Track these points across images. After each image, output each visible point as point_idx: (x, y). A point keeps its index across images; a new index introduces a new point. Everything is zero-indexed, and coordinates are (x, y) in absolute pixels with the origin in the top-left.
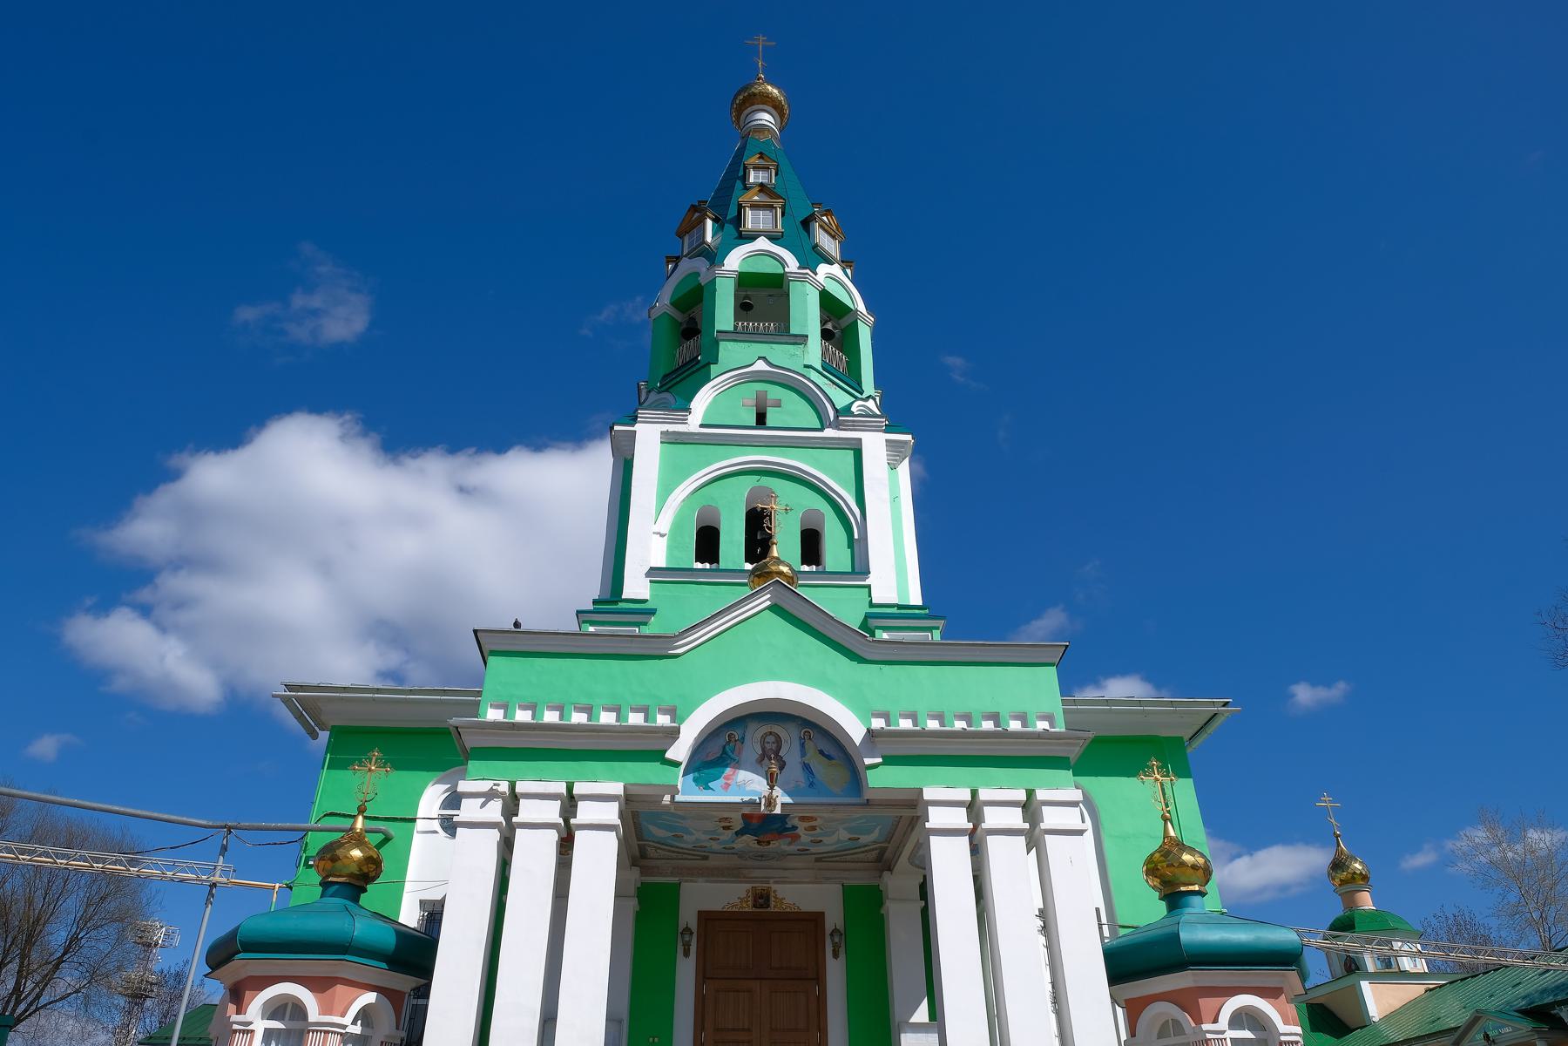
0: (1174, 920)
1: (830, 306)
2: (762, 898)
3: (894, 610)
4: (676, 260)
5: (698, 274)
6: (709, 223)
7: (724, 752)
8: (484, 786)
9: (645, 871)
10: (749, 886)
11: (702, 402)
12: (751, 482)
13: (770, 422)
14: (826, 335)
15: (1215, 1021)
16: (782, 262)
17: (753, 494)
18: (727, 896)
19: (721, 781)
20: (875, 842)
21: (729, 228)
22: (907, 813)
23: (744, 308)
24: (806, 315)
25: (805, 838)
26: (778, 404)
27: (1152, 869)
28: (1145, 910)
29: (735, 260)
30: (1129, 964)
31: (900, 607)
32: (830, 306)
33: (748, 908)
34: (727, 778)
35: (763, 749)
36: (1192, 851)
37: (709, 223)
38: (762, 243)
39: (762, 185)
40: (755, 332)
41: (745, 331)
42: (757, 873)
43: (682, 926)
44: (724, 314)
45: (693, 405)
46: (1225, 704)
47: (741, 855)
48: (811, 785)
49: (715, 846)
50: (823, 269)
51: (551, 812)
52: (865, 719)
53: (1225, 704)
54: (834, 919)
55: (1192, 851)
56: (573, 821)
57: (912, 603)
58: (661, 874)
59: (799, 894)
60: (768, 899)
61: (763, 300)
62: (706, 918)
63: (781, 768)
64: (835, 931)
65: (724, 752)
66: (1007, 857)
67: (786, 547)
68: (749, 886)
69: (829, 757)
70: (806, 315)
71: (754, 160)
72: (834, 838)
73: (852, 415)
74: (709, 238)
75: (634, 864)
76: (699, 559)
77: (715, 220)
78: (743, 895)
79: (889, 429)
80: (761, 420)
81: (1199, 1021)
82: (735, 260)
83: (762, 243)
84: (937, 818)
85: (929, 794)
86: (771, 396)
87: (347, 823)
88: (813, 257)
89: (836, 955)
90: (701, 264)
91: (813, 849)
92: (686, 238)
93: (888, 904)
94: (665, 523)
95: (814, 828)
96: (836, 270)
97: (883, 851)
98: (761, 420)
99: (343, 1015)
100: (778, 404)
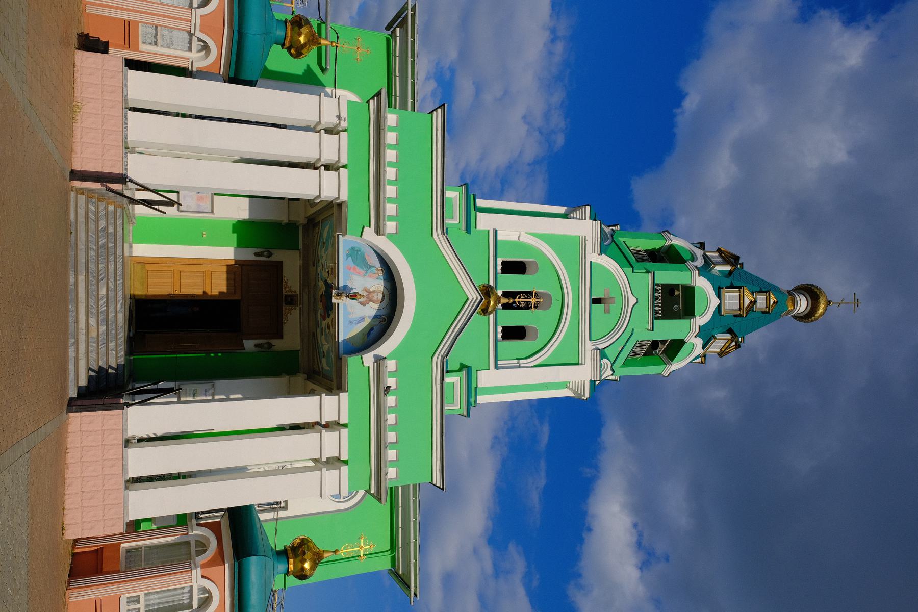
0: (270, 555)
1: (674, 347)
2: (291, 300)
3: (473, 386)
4: (702, 246)
5: (693, 260)
7: (371, 267)
9: (304, 226)
10: (298, 293)
11: (606, 262)
12: (556, 297)
13: (594, 306)
14: (655, 344)
15: (203, 577)
16: (702, 314)
17: (548, 297)
18: (292, 278)
19: (352, 265)
20: (323, 368)
21: (728, 282)
22: (335, 384)
23: (669, 290)
24: (668, 330)
25: (324, 324)
26: (607, 311)
27: (304, 542)
28: (277, 534)
29: (703, 285)
30: (240, 520)
31: (476, 389)
32: (674, 347)
33: (285, 292)
34: (354, 268)
35: (373, 292)
36: (313, 568)
37: (728, 268)
38: (715, 302)
39: (755, 302)
40: (655, 298)
41: (654, 291)
42: (306, 298)
43: (272, 251)
44: (668, 275)
45: (604, 256)
46: (416, 595)
47: (316, 286)
48: (351, 322)
49: (319, 269)
50: (699, 342)
51: (329, 156)
52: (393, 356)
53: (416, 595)
54: (279, 345)
55: (313, 568)
57: (478, 397)
58: (304, 237)
59: (293, 321)
62: (279, 265)
63: (361, 303)
64: (270, 345)
65: (371, 267)
66: (305, 446)
68: (298, 293)
69: (369, 334)
70: (668, 330)
71: (773, 299)
72: (324, 342)
73: (601, 359)
74: (718, 268)
75: (309, 221)
76: (503, 263)
77: (730, 273)
78: (293, 289)
79: (592, 383)
80: (597, 301)
81: (204, 566)
82: (703, 285)
83: (715, 302)
84: (330, 401)
85: (343, 395)
86: (611, 306)
87: (323, 35)
88: (707, 336)
89: (256, 346)
90: (700, 262)
91: (319, 331)
92: (717, 254)
93: (287, 377)
94: (527, 239)
95: (329, 328)
96: (699, 351)
97: (318, 373)
98: (597, 301)
99: (201, 31)
100: (607, 311)
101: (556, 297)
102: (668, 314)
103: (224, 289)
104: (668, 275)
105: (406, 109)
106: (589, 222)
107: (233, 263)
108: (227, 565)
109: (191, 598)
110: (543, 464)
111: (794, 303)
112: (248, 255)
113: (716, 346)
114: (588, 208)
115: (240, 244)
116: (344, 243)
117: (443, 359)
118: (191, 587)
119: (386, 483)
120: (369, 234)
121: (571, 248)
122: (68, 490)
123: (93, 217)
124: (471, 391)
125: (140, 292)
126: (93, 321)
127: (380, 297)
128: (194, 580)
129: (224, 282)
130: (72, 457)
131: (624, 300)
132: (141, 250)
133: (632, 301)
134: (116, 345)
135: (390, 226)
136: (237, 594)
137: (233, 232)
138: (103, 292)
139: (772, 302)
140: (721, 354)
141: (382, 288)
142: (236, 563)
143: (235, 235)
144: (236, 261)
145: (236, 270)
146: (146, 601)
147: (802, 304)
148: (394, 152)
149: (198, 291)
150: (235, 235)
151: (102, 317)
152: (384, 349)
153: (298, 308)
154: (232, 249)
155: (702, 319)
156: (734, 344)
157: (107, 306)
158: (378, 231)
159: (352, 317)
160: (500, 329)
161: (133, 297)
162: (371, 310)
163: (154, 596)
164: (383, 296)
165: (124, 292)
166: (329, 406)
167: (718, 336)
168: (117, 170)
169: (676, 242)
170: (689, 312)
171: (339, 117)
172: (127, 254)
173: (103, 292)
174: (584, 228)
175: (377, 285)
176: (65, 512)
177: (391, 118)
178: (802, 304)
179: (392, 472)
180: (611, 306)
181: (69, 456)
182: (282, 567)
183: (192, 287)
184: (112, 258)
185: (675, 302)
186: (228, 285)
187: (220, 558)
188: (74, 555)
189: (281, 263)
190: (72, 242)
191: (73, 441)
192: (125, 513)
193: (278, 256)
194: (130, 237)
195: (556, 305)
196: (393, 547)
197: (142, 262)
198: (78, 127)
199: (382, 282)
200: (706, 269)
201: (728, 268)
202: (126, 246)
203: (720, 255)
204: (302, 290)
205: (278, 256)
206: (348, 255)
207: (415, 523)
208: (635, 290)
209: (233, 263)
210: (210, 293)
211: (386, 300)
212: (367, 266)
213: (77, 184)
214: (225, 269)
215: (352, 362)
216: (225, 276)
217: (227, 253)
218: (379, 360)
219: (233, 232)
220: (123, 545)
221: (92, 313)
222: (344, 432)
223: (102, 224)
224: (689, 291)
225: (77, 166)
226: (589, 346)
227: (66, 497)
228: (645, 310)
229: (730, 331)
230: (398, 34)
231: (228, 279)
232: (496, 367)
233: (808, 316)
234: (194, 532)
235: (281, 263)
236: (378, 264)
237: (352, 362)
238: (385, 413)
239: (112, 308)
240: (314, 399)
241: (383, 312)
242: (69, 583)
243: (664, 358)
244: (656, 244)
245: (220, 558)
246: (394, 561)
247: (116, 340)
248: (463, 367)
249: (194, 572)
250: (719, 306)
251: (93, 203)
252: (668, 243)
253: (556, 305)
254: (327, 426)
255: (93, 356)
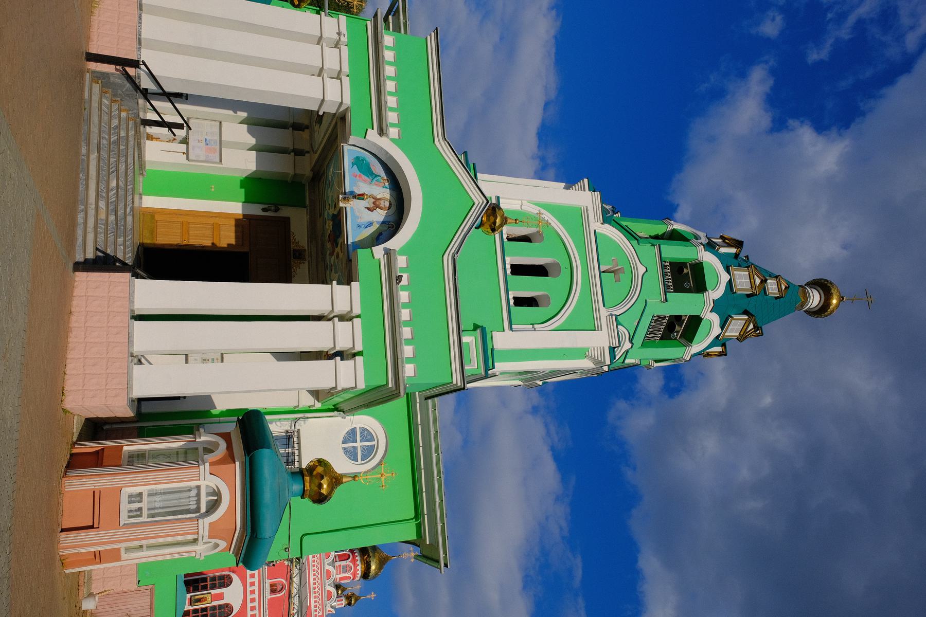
2: (299, 255)
3: (490, 347)
6: (67, 571)
8: (344, 30)
11: (609, 231)
12: (564, 265)
17: (557, 266)
19: (358, 173)
24: (683, 304)
26: (618, 280)
29: (709, 259)
31: (492, 350)
33: (293, 246)
35: (380, 199)
38: (725, 277)
40: (664, 274)
41: (663, 267)
45: (606, 226)
46: (446, 565)
48: (360, 226)
50: (715, 319)
51: (342, 307)
52: (403, 251)
53: (446, 565)
56: (338, 358)
60: (299, 258)
61: (685, 277)
62: (286, 221)
67: (528, 286)
70: (683, 304)
76: (513, 266)
82: (709, 259)
83: (725, 277)
84: (341, 291)
86: (621, 275)
88: (724, 309)
90: (704, 240)
101: (564, 265)
102: (679, 288)
103: (233, 241)
104: (675, 252)
105: (400, 32)
106: (588, 194)
107: (241, 217)
108: (237, 463)
109: (198, 502)
110: (581, 601)
111: (806, 297)
112: (256, 210)
113: (736, 327)
114: (586, 180)
115: (246, 202)
116: (348, 152)
117: (453, 256)
118: (198, 487)
119: (404, 381)
120: (373, 135)
121: (574, 218)
122: (71, 355)
123: (106, 110)
124: (488, 356)
125: (147, 241)
126: (102, 204)
127: (387, 204)
128: (202, 477)
129: (233, 235)
130: (76, 321)
131: (633, 270)
132: (150, 202)
133: (642, 270)
134: (125, 241)
135: (393, 132)
136: (248, 492)
137: (241, 187)
138: (113, 184)
139: (783, 287)
140: (741, 338)
141: (388, 196)
142: (248, 459)
143: (243, 190)
144: (244, 215)
145: (244, 225)
146: (149, 502)
147: (815, 299)
148: (395, 99)
149: (207, 242)
150: (243, 190)
151: (111, 208)
152: (395, 243)
153: (307, 263)
154: (241, 204)
155: (716, 292)
156: (751, 326)
157: (117, 197)
158: (381, 132)
159: (360, 219)
160: (508, 266)
161: (142, 245)
162: (379, 216)
163: (158, 498)
164: (390, 204)
165: (133, 238)
166: (341, 296)
167: (735, 316)
168: (132, 57)
169: (677, 226)
170: (700, 287)
171: (339, 34)
172: (136, 204)
173: (113, 184)
174: (584, 198)
175: (384, 193)
176: (66, 377)
177: (388, 39)
178: (815, 299)
179: (409, 370)
180: (621, 275)
181: (72, 335)
182: (297, 487)
183: (200, 238)
184: (123, 159)
185: (685, 277)
186: (237, 237)
187: (230, 457)
188: (72, 455)
189: (289, 218)
190: (86, 117)
191: (77, 304)
192: (129, 386)
193: (285, 212)
194: (140, 187)
195: (565, 273)
196: (418, 514)
197: (152, 214)
198: (95, 20)
199: (388, 191)
200: (711, 246)
201: (733, 250)
202: (137, 197)
203: (724, 241)
204: (310, 243)
205: (285, 212)
206: (353, 164)
207: (439, 481)
208: (645, 265)
209: (241, 217)
210: (218, 245)
211: (393, 209)
212: (373, 175)
213: (93, 66)
214: (233, 223)
215: (362, 254)
216: (233, 229)
217: (236, 208)
218: (388, 252)
219: (241, 187)
220: (125, 448)
221: (102, 197)
222: (357, 321)
223: (115, 123)
224: (698, 268)
225: (93, 50)
226: (604, 312)
227: (68, 361)
228: (655, 281)
229: (746, 312)
230: (391, 21)
231: (236, 232)
232: (511, 328)
233: (822, 310)
234: (203, 438)
235: (289, 218)
236: (383, 174)
237: (362, 254)
238: (398, 308)
239: (121, 205)
240: (327, 287)
241: (391, 219)
242: (65, 472)
243: (683, 341)
244: (660, 228)
245: (230, 457)
246: (419, 528)
247: (125, 237)
248: (476, 327)
249: (202, 467)
250: (730, 281)
251: (107, 98)
252: (670, 228)
253: (565, 273)
254: (341, 354)
255: (101, 237)
